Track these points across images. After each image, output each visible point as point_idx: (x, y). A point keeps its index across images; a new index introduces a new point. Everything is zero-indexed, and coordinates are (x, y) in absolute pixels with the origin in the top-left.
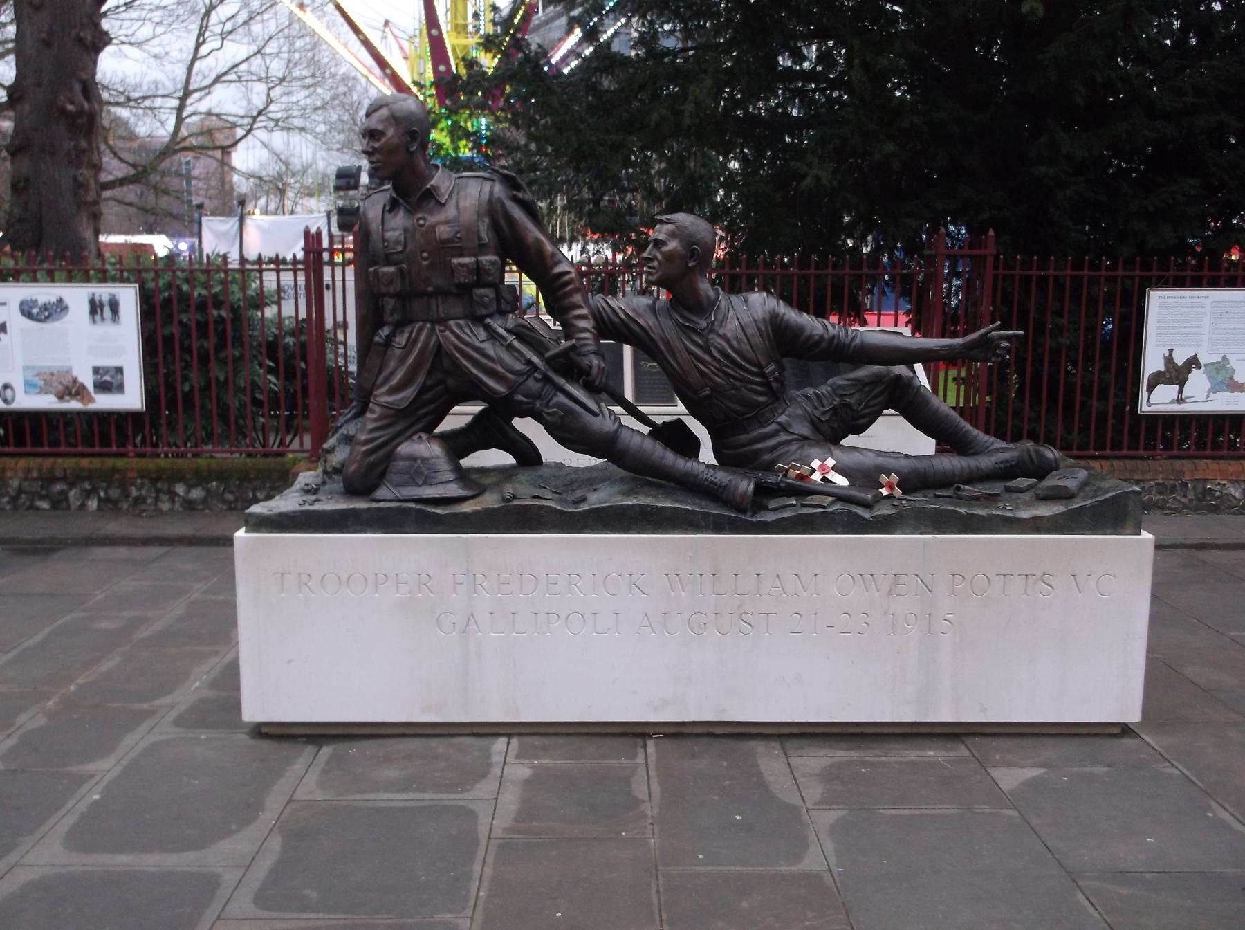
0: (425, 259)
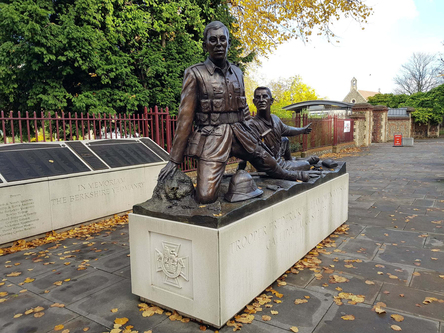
0: (230, 97)
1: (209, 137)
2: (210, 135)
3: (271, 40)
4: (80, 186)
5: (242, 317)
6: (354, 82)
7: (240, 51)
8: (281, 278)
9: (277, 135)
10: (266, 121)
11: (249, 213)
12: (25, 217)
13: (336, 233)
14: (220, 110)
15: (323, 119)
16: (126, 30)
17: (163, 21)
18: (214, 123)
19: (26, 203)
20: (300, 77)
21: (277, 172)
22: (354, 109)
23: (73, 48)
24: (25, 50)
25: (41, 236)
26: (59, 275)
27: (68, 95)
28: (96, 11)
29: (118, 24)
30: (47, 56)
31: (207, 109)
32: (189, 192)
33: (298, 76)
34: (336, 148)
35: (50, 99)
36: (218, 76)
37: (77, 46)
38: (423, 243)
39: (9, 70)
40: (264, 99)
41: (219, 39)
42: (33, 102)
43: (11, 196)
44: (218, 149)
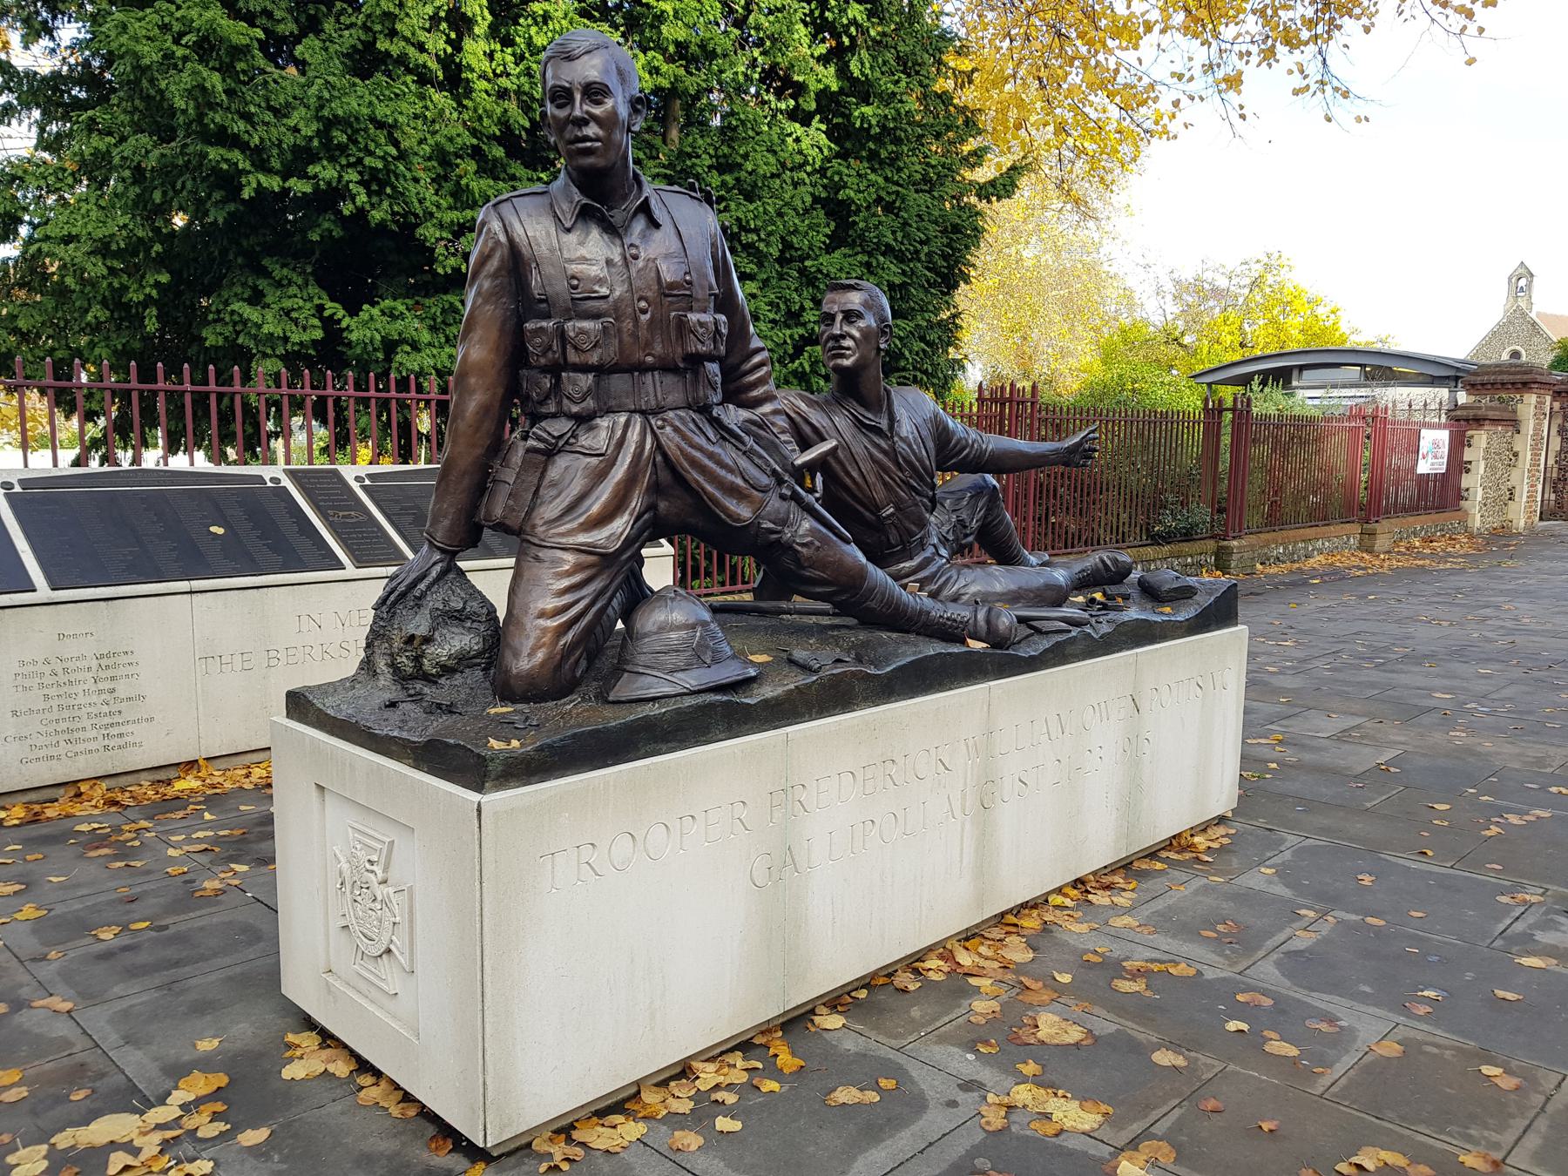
0: (644, 312)
1: (556, 458)
2: (560, 451)
3: (1128, 119)
4: (304, 619)
5: (603, 1125)
6: (1521, 281)
7: (978, 156)
8: (835, 1001)
10: (862, 410)
11: (661, 746)
12: (105, 709)
13: (1164, 854)
14: (594, 359)
15: (1329, 420)
16: (526, 87)
17: (664, 51)
18: (575, 409)
19: (110, 662)
20: (1283, 261)
21: (873, 604)
22: (1473, 385)
23: (337, 153)
24: (189, 161)
25: (162, 775)
26: (128, 907)
27: (333, 308)
28: (427, 25)
29: (501, 68)
30: (251, 177)
31: (544, 354)
32: (474, 657)
33: (1276, 255)
34: (1373, 534)
35: (269, 317)
36: (595, 233)
37: (351, 146)
38: (1501, 927)
39: (143, 225)
40: (846, 328)
41: (578, 97)
42: (221, 334)
43: (61, 636)
44: (587, 503)
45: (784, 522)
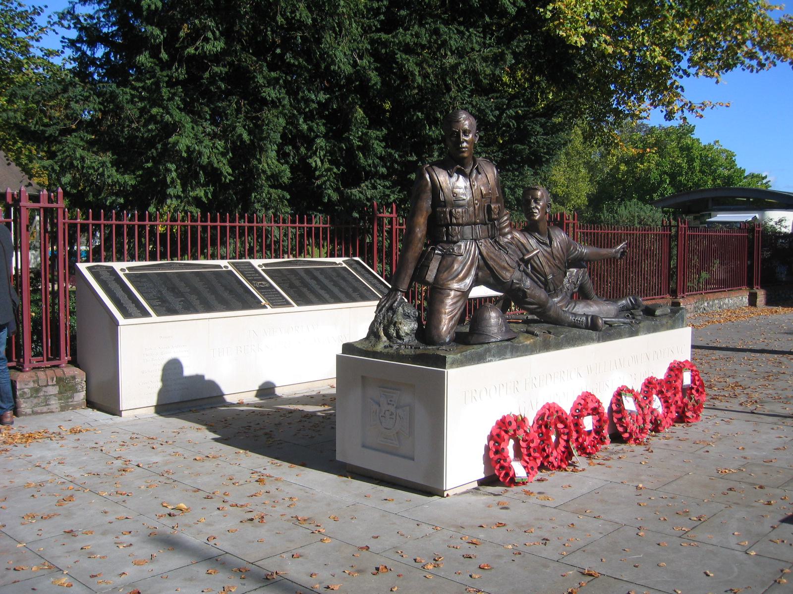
9: (557, 256)
45: (520, 280)
